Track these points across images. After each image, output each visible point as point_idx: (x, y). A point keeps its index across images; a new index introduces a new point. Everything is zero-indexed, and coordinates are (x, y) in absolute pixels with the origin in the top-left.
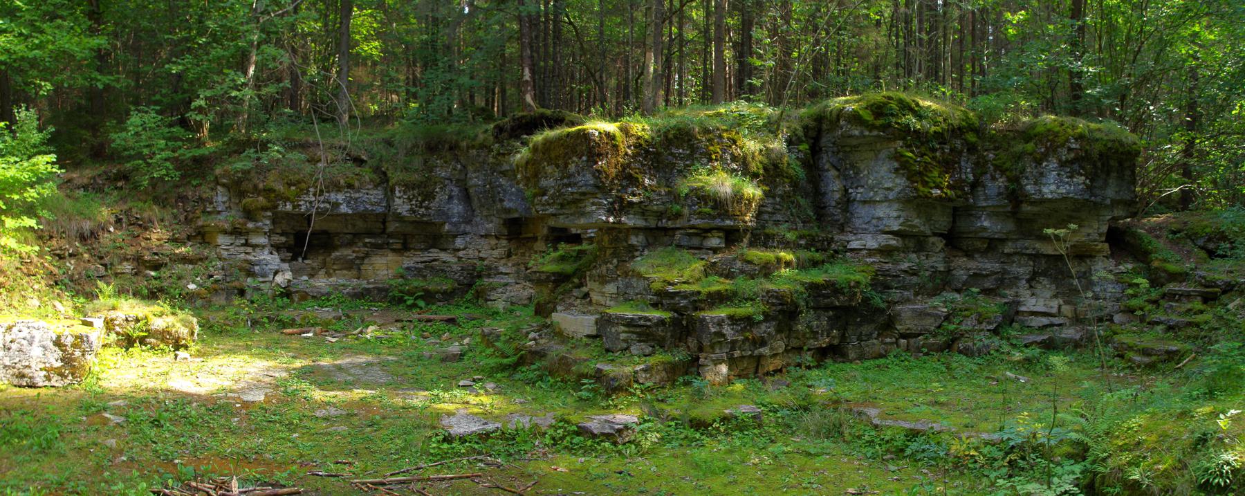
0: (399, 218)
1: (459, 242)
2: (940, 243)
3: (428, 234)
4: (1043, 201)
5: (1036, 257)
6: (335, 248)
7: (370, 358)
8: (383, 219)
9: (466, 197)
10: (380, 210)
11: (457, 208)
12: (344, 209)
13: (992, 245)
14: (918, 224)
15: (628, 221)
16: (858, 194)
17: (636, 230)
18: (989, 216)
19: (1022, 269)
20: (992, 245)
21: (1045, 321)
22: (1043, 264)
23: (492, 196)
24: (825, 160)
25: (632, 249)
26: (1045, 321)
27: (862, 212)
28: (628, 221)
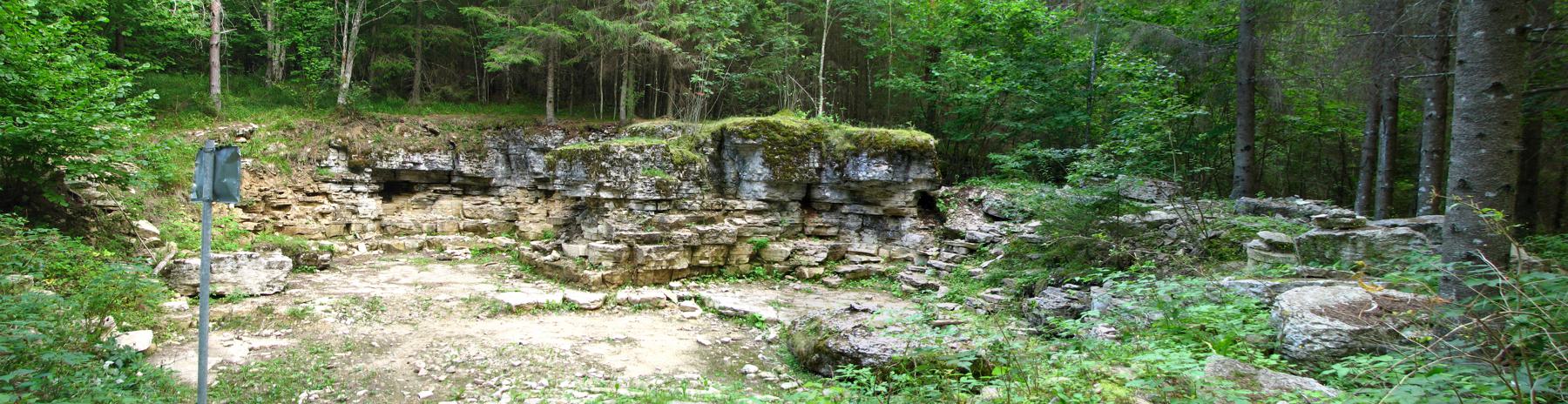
0: (461, 174)
1: (502, 191)
2: (795, 206)
3: (481, 186)
4: (859, 182)
5: (864, 216)
6: (414, 193)
7: (923, 137)
8: (449, 174)
9: (508, 161)
10: (449, 168)
11: (501, 168)
12: (423, 167)
13: (834, 208)
14: (778, 195)
15: (604, 195)
16: (746, 176)
17: (608, 200)
18: (832, 188)
19: (853, 222)
20: (834, 208)
21: (864, 258)
22: (869, 222)
23: (525, 164)
24: (725, 155)
25: (607, 210)
26: (864, 258)
27: (746, 186)
28: (604, 195)
